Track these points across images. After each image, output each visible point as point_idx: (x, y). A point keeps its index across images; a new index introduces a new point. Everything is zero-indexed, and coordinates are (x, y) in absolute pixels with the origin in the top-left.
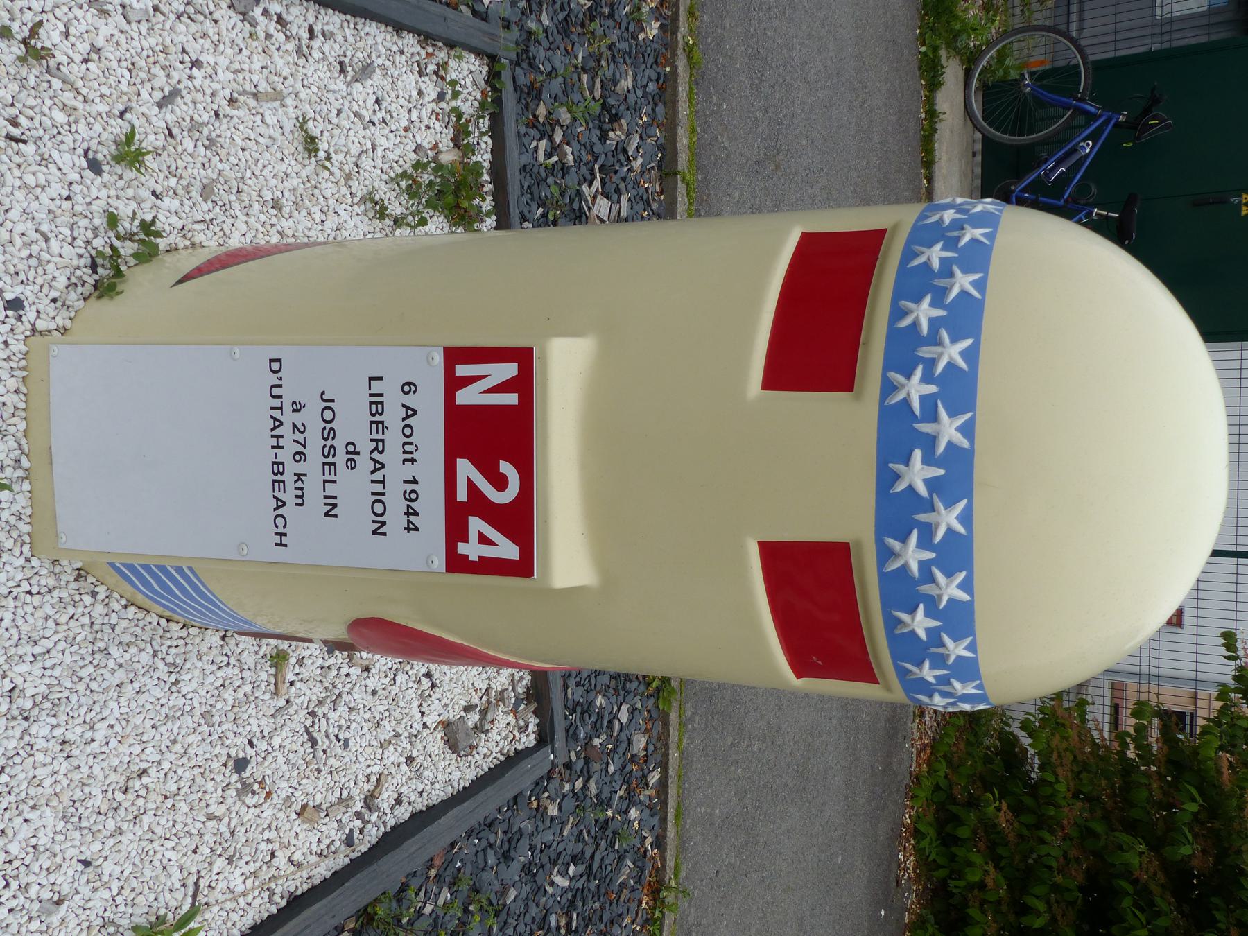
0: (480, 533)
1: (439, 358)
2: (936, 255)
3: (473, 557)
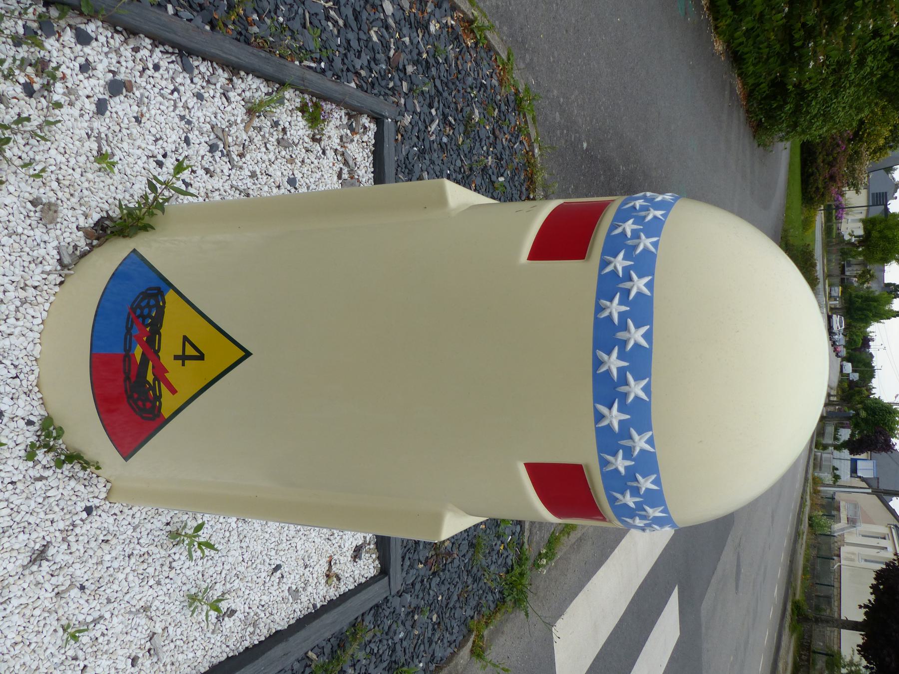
2: (629, 226)
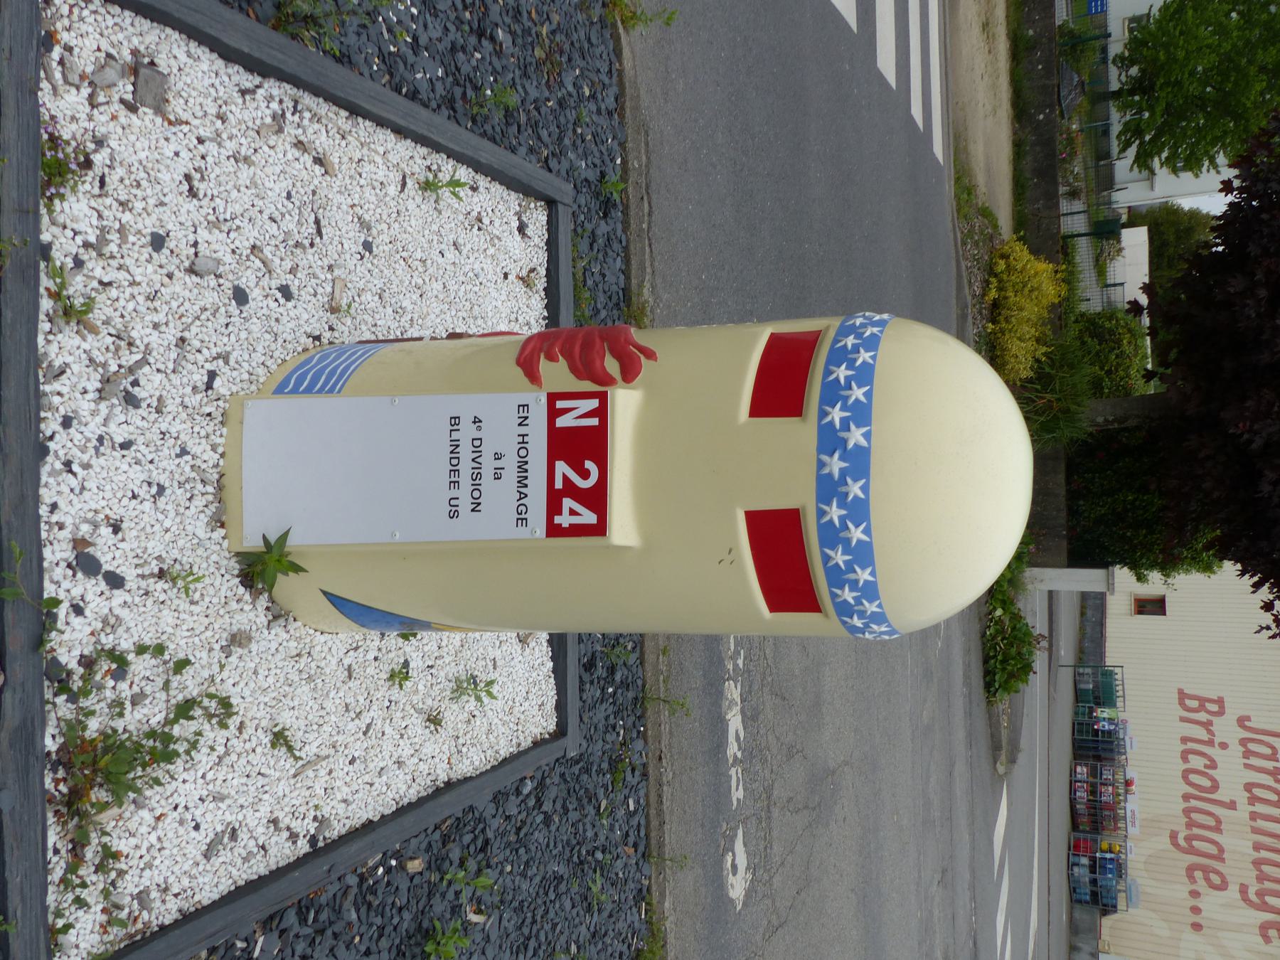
0: (570, 509)
1: (544, 400)
2: (850, 341)
3: (565, 525)
